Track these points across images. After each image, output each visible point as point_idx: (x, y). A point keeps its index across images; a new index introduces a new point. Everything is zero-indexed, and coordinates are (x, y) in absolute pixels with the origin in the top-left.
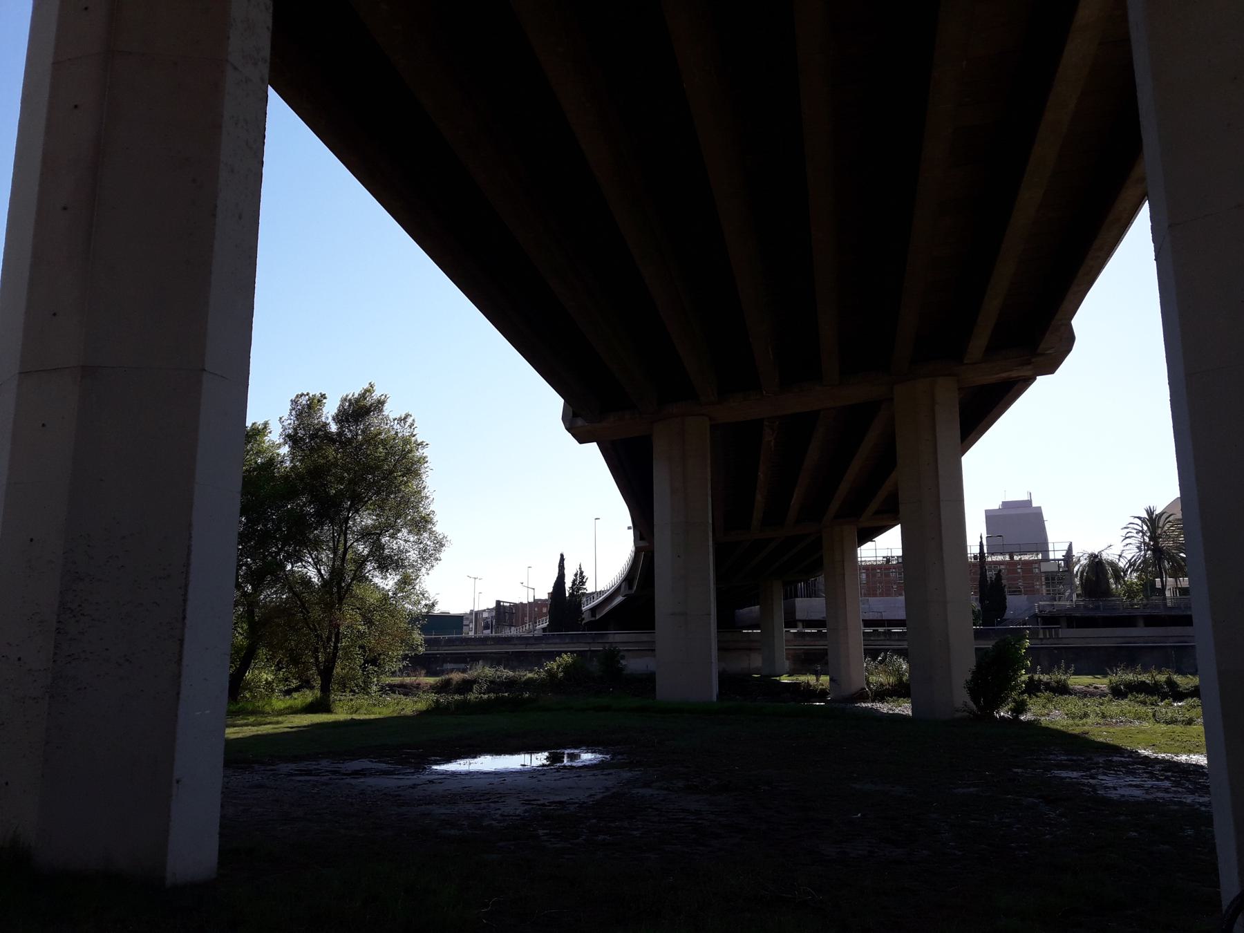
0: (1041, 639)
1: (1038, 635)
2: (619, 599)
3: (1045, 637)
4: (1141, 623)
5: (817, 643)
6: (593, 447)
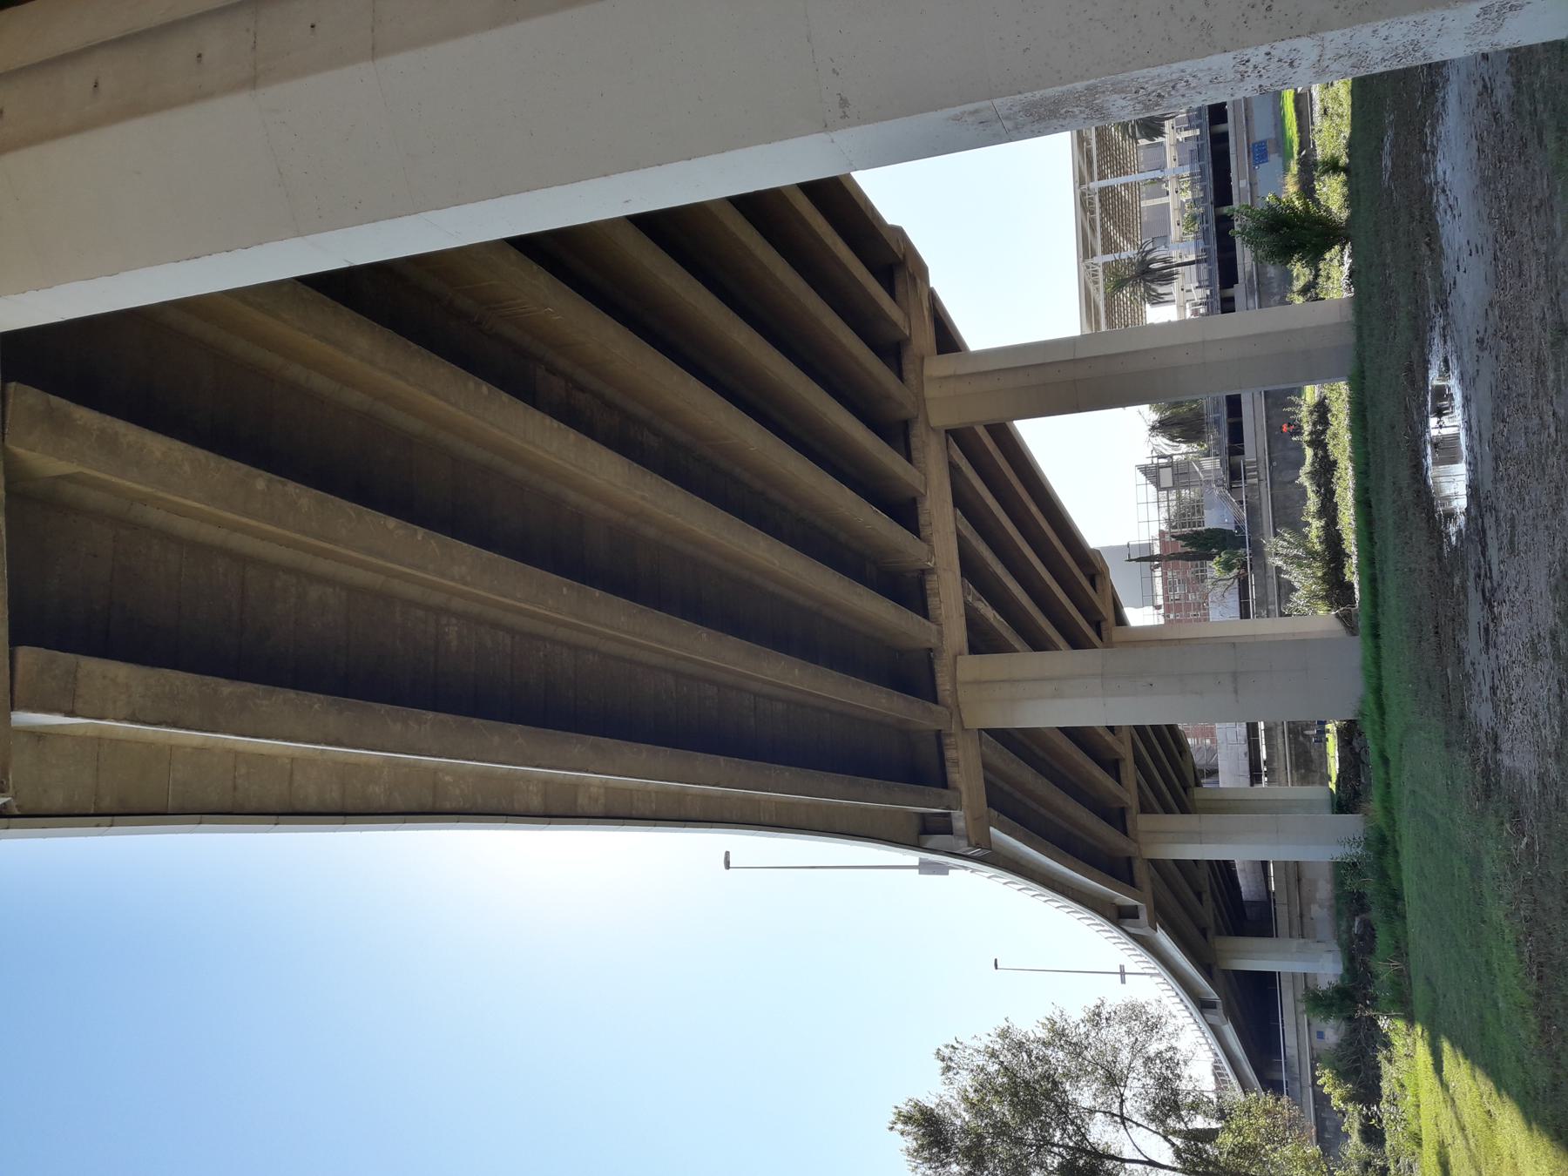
0: (1259, 480)
1: (1254, 484)
2: (1229, 1031)
3: (1258, 476)
4: (1221, 128)
5: (1281, 753)
6: (931, 286)
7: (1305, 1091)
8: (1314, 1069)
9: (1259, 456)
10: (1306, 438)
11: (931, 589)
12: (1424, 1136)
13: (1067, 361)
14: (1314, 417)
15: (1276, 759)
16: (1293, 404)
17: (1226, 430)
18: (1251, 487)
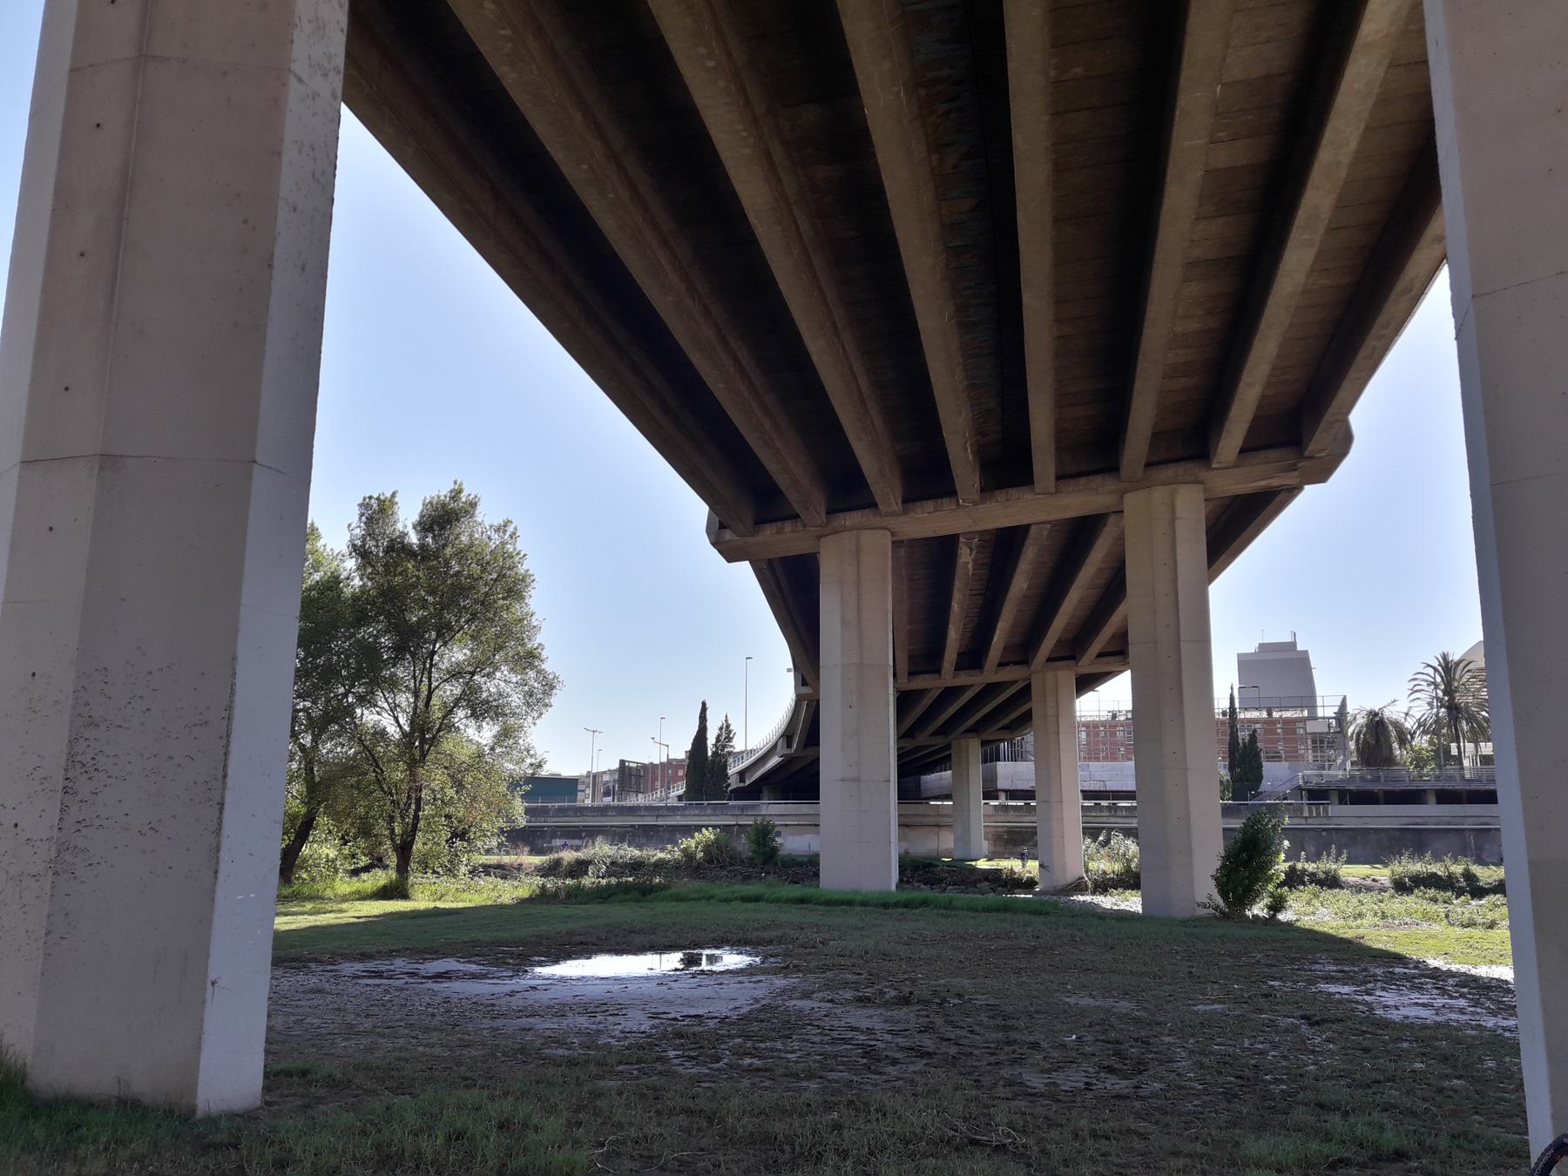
0: (1306, 818)
2: (775, 761)
3: (1311, 816)
5: (1027, 819)
7: (731, 818)
8: (714, 827)
9: (1335, 819)
10: (1299, 866)
11: (942, 503)
12: (1495, 931)
13: (1179, 635)
14: (1321, 874)
15: (1017, 814)
16: (1339, 854)
17: (1365, 788)
18: (1299, 809)
